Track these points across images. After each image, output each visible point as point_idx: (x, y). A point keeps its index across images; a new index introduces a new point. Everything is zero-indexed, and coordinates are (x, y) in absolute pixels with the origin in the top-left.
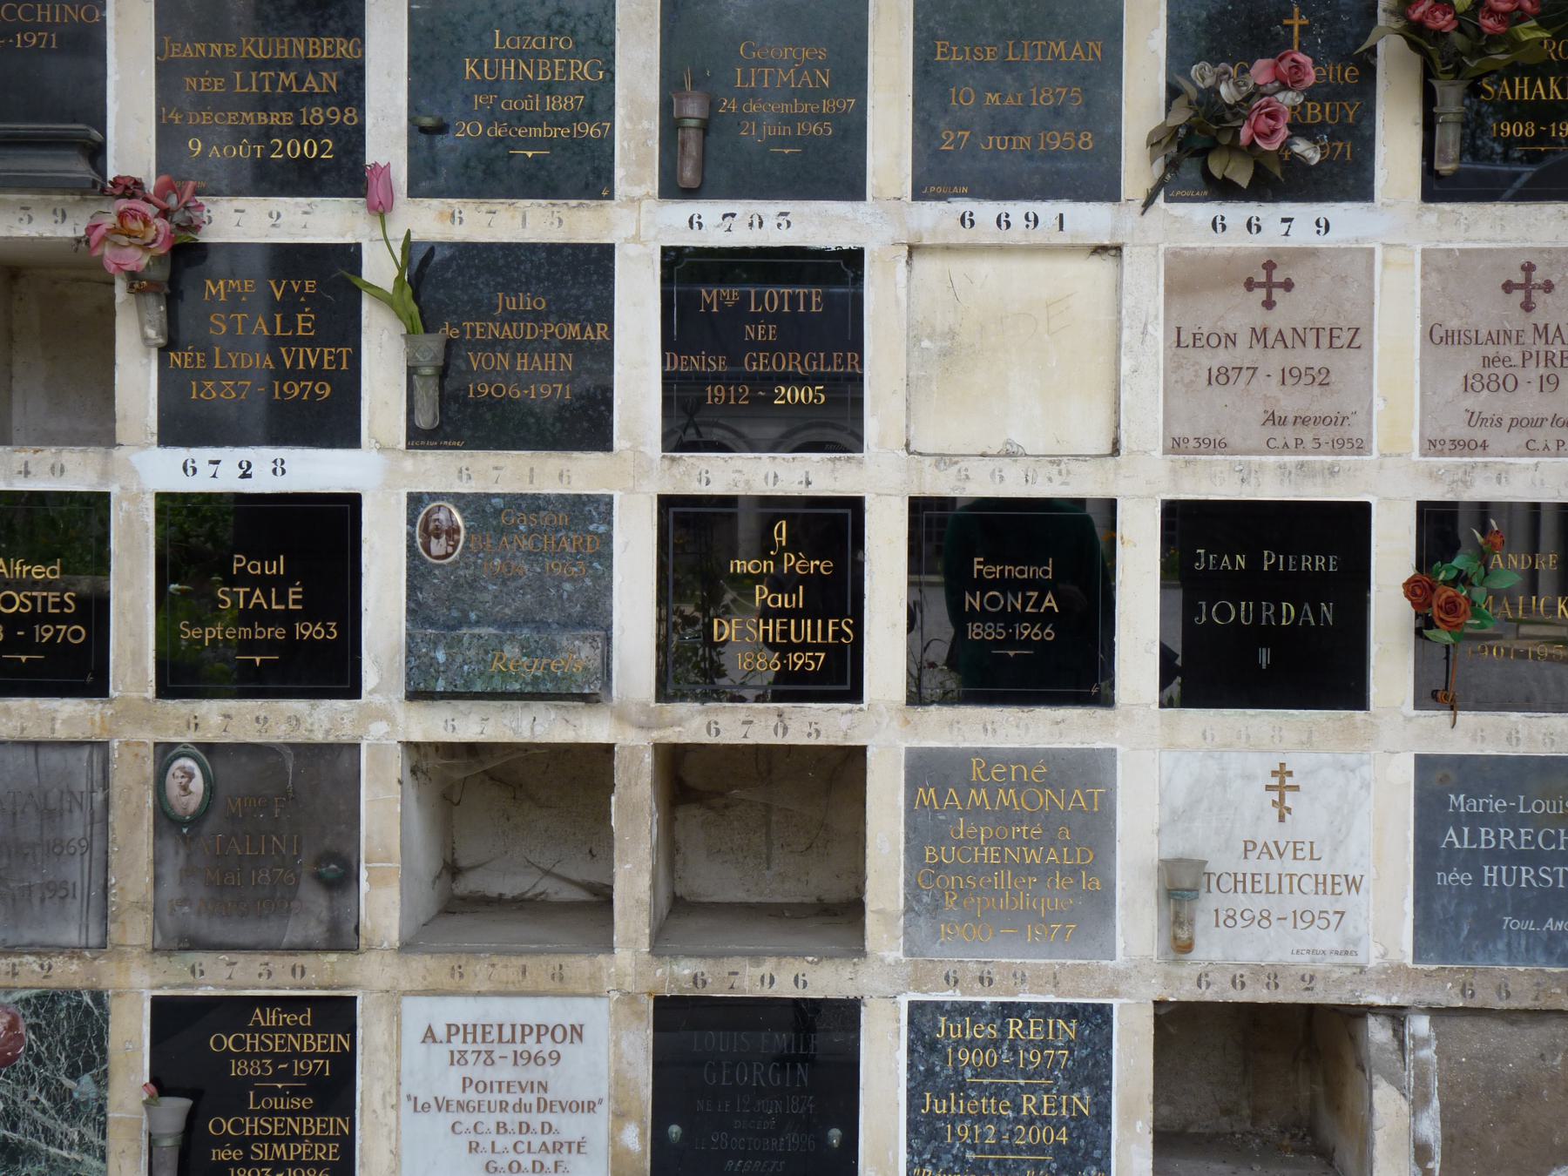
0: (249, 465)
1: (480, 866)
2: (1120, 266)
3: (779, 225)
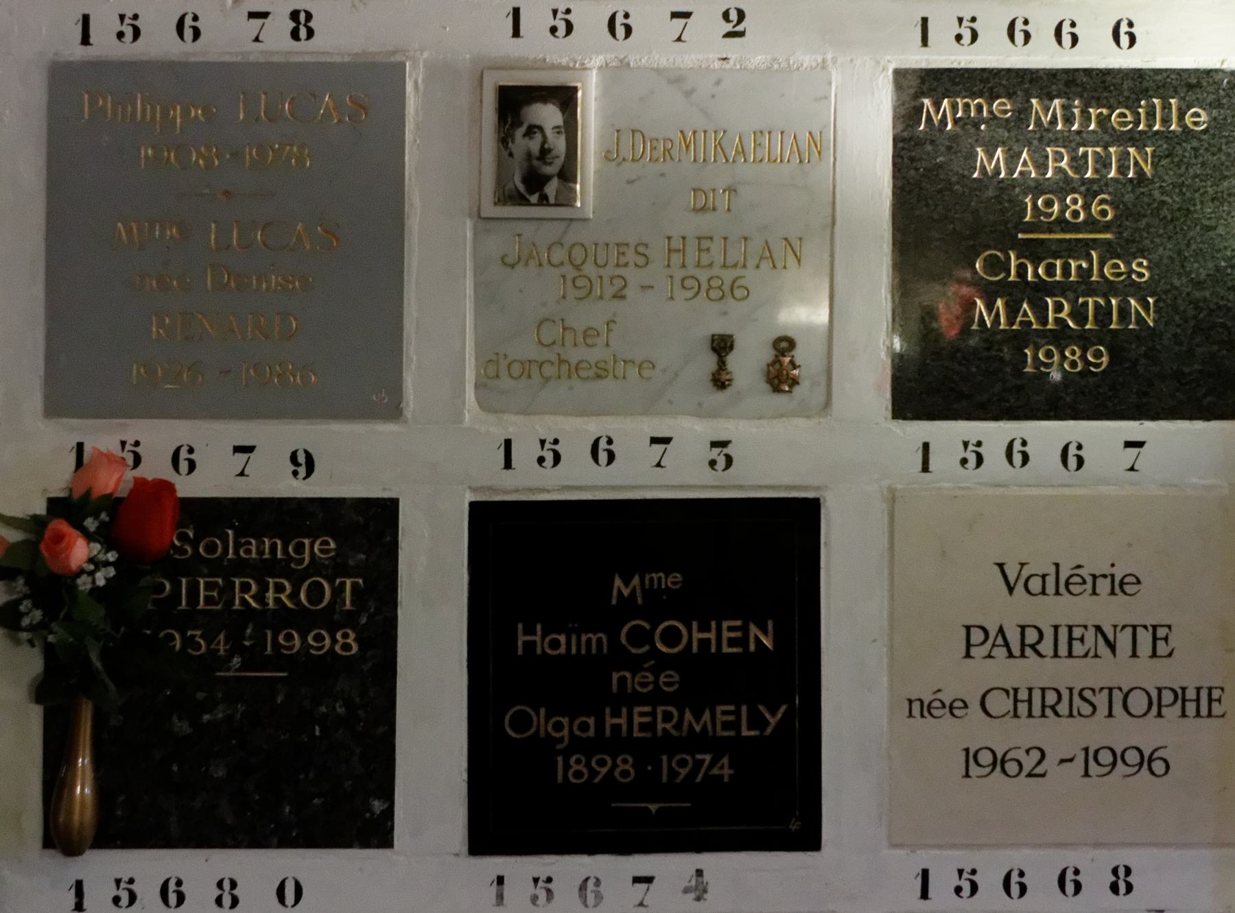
0: (741, 15)
2: (1040, 717)
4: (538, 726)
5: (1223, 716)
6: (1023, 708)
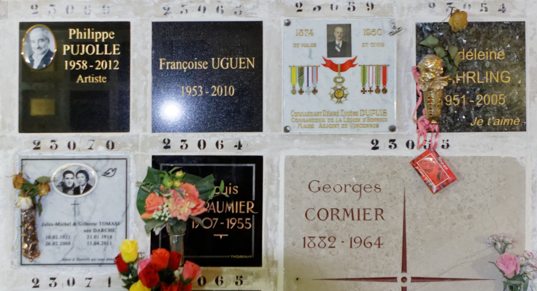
0: (377, 142)
1: (404, 190)
5: (370, 220)
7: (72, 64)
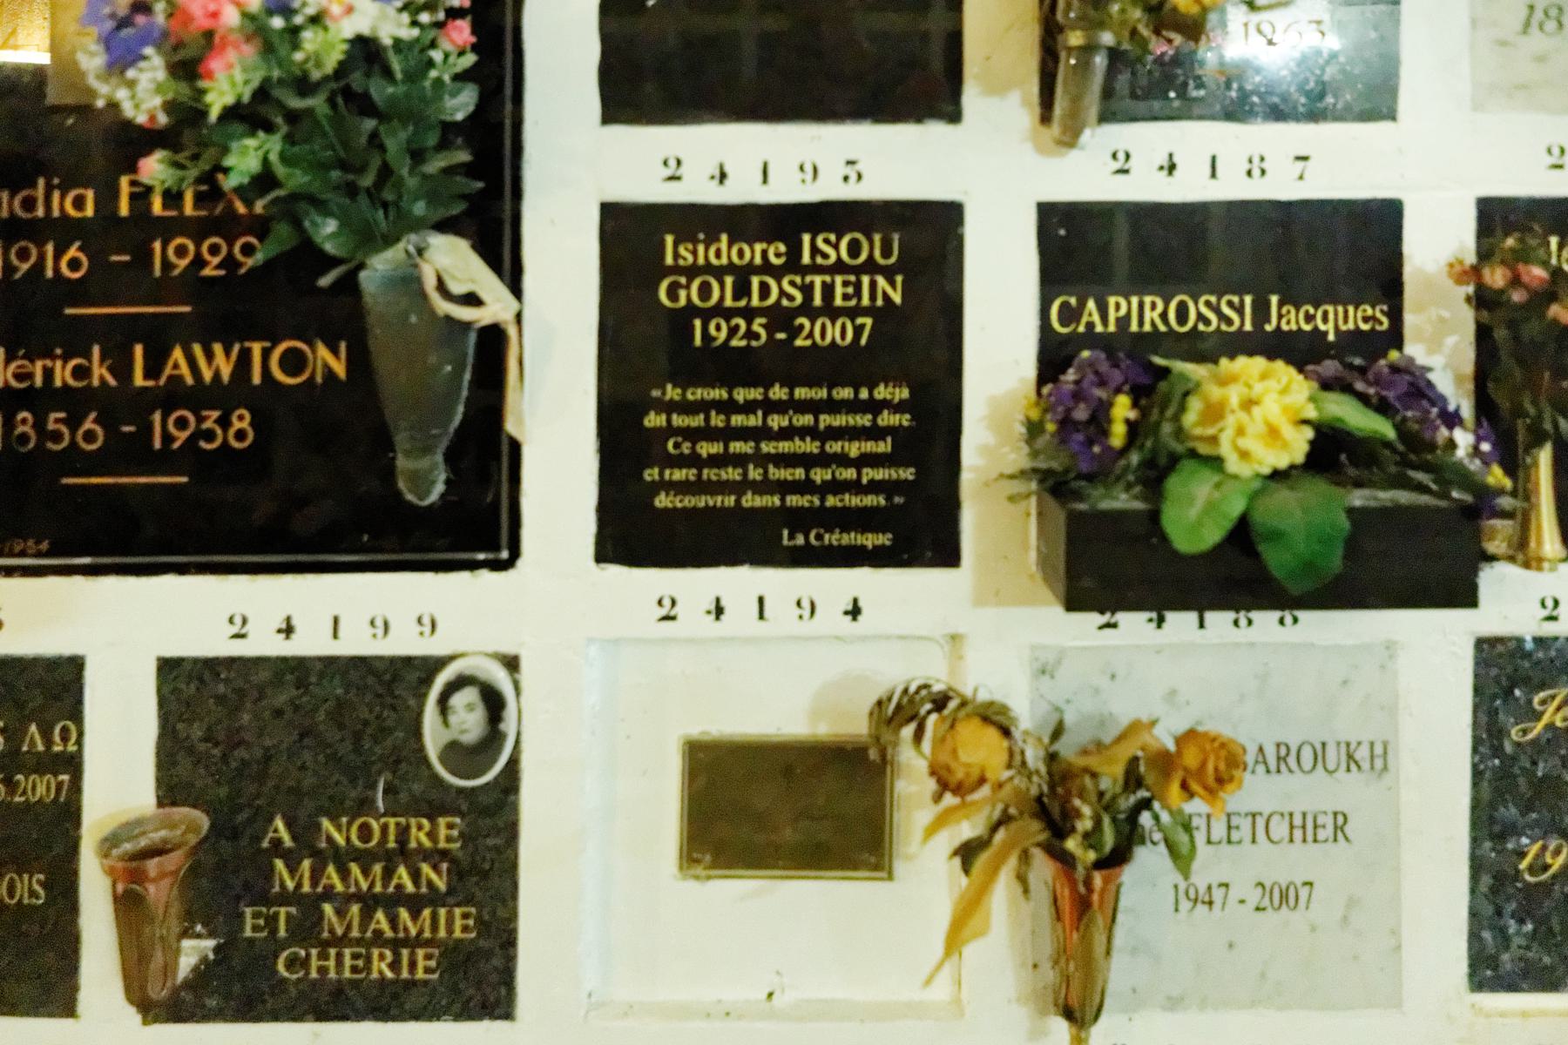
3: (846, 179)
4: (22, 896)
6: (1298, 834)
7: (718, 328)
